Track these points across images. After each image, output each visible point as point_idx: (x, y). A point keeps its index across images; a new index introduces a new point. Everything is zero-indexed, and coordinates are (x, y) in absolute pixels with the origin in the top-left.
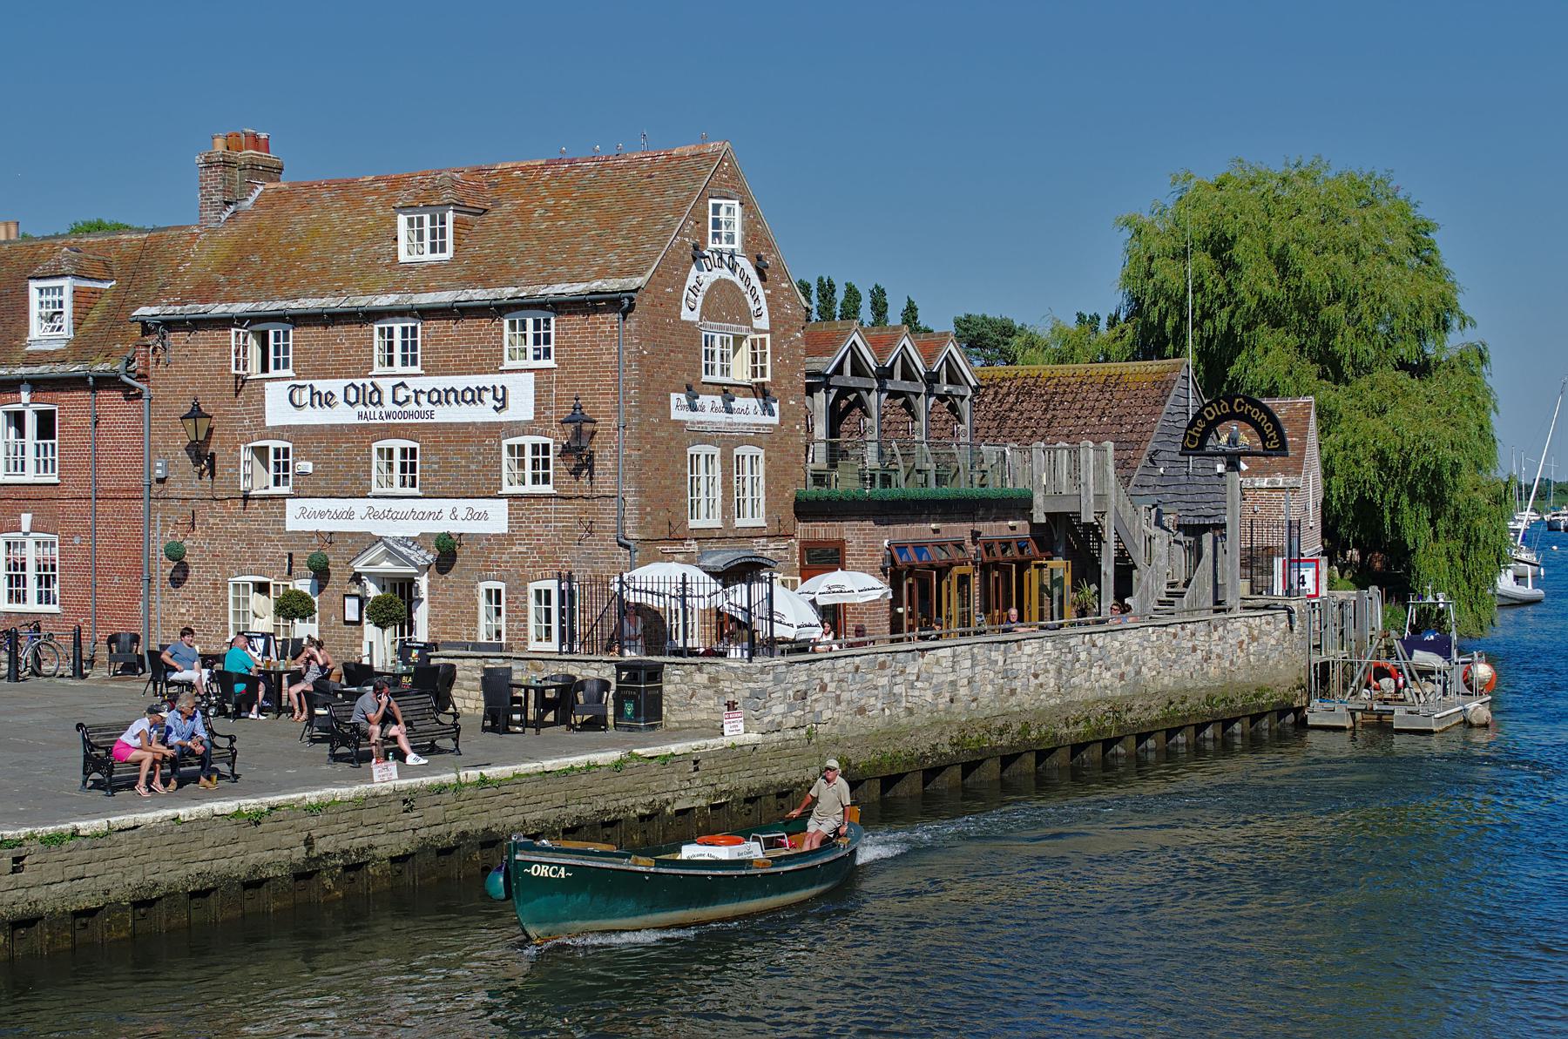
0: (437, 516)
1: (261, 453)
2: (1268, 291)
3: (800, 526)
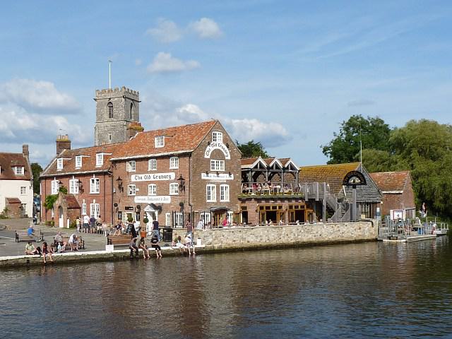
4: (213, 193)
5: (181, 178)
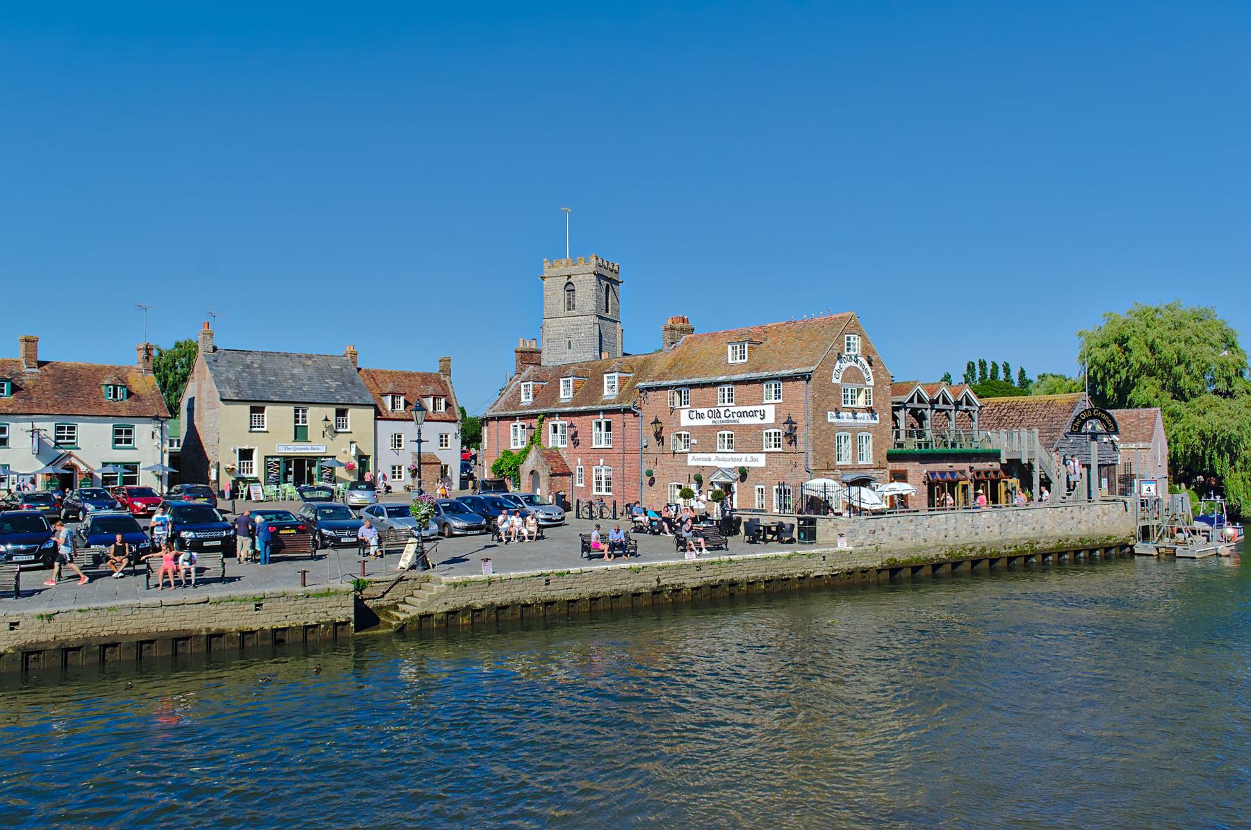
0: (740, 460)
1: (679, 436)
2: (1144, 360)
3: (890, 464)
4: (847, 449)
5: (789, 422)
